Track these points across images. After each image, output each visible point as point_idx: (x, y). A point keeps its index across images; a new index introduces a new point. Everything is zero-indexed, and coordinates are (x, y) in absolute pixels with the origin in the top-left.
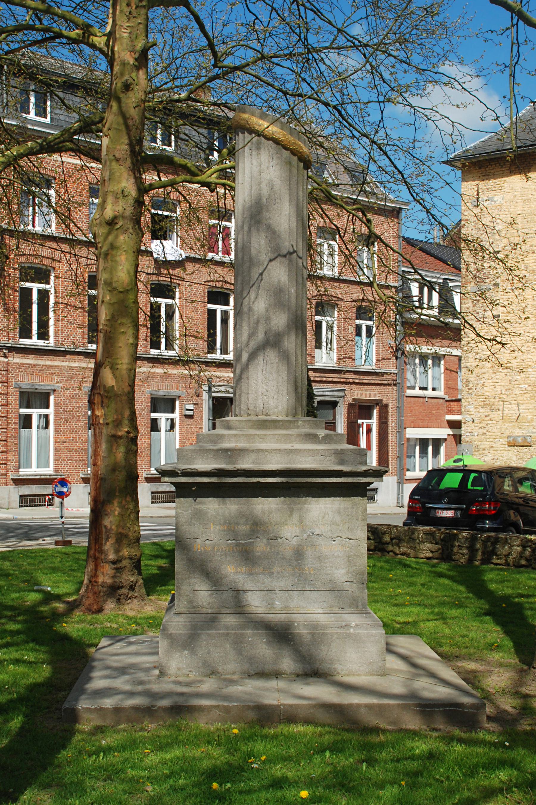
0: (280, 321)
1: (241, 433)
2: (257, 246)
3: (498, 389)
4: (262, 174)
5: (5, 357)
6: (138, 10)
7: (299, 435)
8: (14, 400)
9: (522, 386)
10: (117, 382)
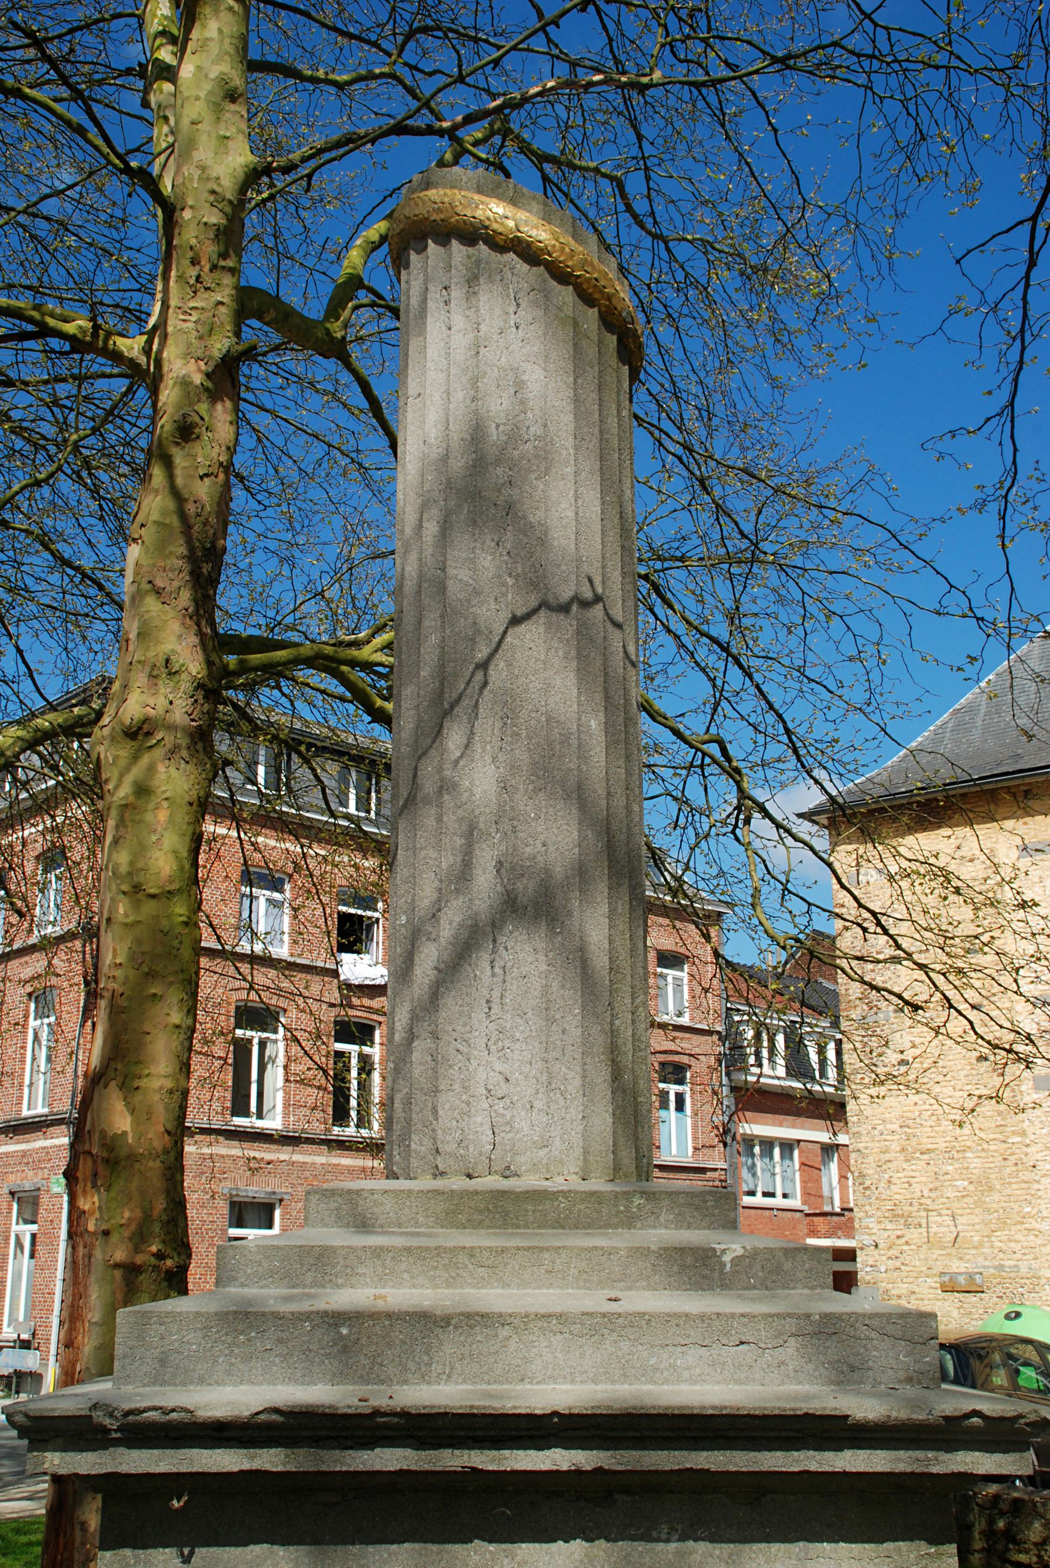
0: (555, 837)
1: (398, 1242)
2: (464, 574)
3: (917, 1188)
4: (482, 350)
6: (216, 275)
7: (640, 1252)
9: (959, 1183)
10: (136, 1123)
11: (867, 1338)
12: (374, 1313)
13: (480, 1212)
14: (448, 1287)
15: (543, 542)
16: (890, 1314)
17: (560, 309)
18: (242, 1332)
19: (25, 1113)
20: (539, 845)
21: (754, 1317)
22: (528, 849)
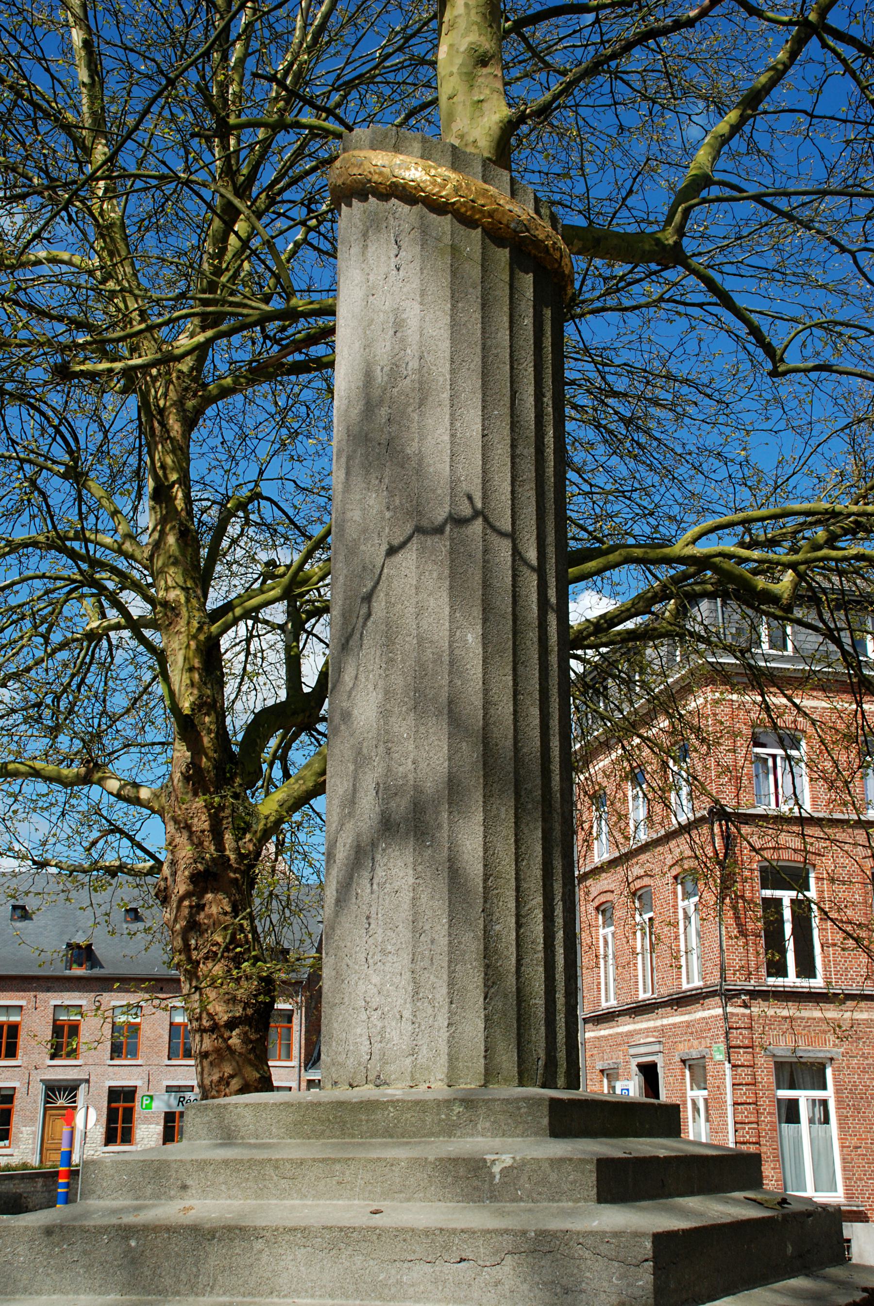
5: (746, 1006)
7: (419, 1163)
8: (766, 1075)
11: (581, 1258)
12: (156, 1226)
13: (322, 1122)
14: (256, 1198)
15: (419, 471)
16: (604, 1233)
17: (439, 240)
18: (58, 1245)
19: (685, 986)
20: (410, 763)
21: (474, 1233)
22: (401, 769)
